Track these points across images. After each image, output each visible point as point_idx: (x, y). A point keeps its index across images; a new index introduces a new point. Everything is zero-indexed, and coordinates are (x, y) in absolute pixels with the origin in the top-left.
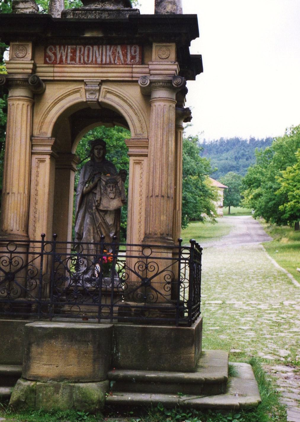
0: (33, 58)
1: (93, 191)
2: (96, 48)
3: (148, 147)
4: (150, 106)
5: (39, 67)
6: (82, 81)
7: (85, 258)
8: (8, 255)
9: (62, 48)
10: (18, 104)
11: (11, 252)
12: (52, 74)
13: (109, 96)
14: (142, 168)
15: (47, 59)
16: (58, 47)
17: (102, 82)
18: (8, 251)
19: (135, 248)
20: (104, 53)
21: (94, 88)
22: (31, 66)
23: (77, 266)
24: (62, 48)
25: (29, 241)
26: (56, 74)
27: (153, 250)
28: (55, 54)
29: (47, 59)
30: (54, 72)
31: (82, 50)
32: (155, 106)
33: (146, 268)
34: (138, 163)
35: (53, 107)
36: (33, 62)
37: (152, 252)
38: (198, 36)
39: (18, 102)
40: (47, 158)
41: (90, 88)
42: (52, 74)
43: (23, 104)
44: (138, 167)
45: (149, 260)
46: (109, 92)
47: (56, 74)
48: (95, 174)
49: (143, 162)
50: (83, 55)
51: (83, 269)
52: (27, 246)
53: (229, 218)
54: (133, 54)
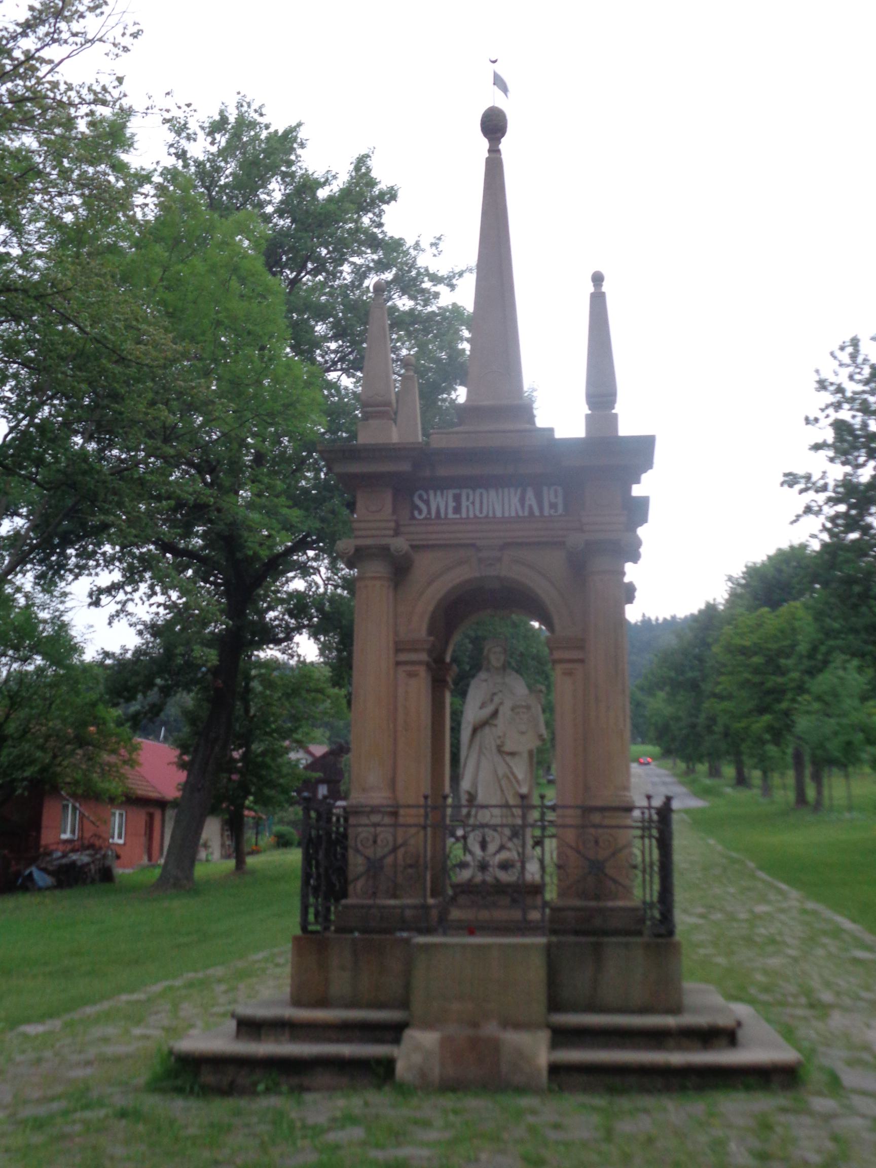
0: (395, 511)
1: (491, 722)
2: (492, 493)
3: (398, 650)
6: (473, 545)
7: (495, 830)
8: (372, 830)
11: (375, 825)
15: (416, 513)
16: (431, 493)
17: (506, 546)
19: (569, 812)
20: (506, 499)
22: (392, 525)
23: (484, 845)
25: (398, 806)
28: (427, 503)
31: (485, 496)
34: (569, 673)
36: (394, 518)
40: (422, 671)
45: (600, 831)
50: (473, 503)
51: (492, 847)
52: (395, 814)
53: (475, 784)
54: (553, 500)
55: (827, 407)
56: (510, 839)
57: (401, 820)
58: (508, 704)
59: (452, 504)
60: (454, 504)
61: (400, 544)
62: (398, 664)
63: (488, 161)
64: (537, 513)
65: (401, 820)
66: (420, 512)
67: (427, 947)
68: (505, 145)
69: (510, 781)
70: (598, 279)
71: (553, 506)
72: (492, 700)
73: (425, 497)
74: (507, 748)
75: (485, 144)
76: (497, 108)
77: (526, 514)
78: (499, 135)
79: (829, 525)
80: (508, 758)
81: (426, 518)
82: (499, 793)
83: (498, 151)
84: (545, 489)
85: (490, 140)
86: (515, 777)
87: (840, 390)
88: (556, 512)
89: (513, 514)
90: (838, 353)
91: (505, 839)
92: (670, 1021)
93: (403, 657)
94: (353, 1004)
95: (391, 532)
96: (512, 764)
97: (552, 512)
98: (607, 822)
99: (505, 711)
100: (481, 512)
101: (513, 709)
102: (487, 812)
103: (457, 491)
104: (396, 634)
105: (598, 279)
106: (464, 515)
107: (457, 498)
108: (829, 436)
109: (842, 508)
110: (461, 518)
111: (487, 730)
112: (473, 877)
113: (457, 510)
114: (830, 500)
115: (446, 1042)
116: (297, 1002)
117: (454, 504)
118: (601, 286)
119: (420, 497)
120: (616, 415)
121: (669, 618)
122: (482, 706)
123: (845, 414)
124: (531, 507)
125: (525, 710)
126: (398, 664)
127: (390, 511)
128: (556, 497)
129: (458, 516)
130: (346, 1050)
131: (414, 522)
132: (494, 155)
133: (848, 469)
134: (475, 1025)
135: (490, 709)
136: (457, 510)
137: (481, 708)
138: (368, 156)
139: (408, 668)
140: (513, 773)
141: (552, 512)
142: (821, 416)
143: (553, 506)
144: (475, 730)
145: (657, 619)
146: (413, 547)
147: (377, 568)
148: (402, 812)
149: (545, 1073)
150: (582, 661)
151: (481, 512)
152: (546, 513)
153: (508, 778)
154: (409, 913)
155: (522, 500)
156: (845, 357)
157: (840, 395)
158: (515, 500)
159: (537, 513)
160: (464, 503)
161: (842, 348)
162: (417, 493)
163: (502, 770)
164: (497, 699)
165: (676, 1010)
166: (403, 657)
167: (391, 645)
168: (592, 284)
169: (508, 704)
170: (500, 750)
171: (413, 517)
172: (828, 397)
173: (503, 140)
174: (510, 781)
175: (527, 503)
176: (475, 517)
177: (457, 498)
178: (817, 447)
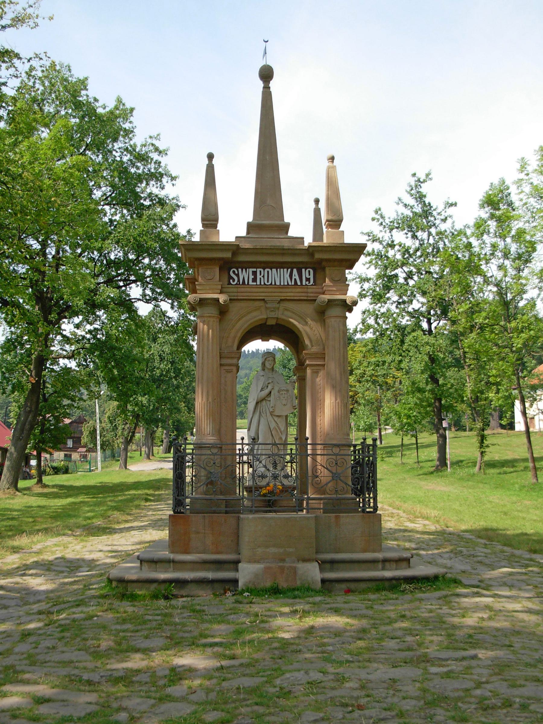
2: (274, 270)
15: (231, 281)
22: (220, 287)
28: (238, 275)
50: (263, 276)
54: (308, 277)
56: (260, 462)
58: (276, 389)
59: (251, 277)
64: (299, 283)
66: (234, 281)
67: (343, 516)
71: (308, 280)
73: (236, 272)
77: (293, 283)
81: (237, 284)
82: (271, 437)
84: (303, 270)
86: (280, 429)
92: (379, 556)
93: (224, 361)
94: (204, 552)
97: (307, 283)
100: (268, 282)
103: (255, 270)
106: (258, 283)
107: (254, 273)
113: (254, 280)
119: (234, 272)
121: (255, 351)
122: (262, 390)
124: (295, 279)
126: (221, 365)
130: (210, 575)
131: (230, 286)
135: (267, 391)
136: (254, 280)
140: (278, 427)
141: (307, 283)
143: (308, 280)
145: (248, 351)
149: (320, 584)
151: (268, 282)
152: (304, 283)
158: (287, 276)
159: (299, 283)
160: (258, 276)
162: (232, 271)
164: (270, 387)
165: (380, 550)
166: (224, 361)
169: (276, 389)
170: (272, 414)
171: (229, 283)
176: (265, 284)
177: (254, 273)
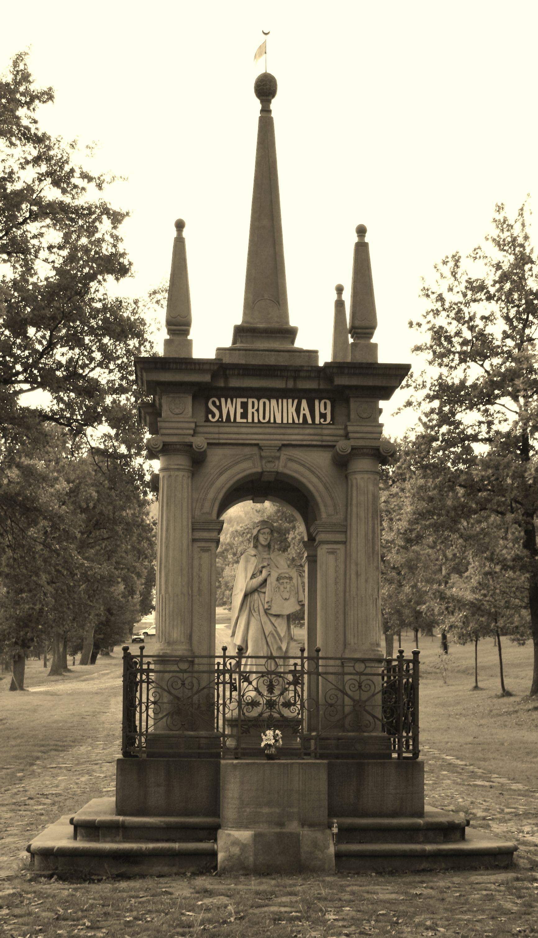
3: (193, 530)
4: (346, 477)
5: (201, 426)
6: (257, 445)
9: (229, 400)
10: (177, 476)
12: (216, 436)
13: (290, 464)
14: (336, 560)
15: (210, 416)
18: (178, 669)
19: (331, 662)
21: (273, 454)
22: (193, 425)
24: (229, 400)
26: (222, 436)
27: (368, 665)
28: (219, 408)
29: (210, 416)
30: (219, 433)
32: (356, 479)
33: (360, 687)
34: (333, 552)
35: (217, 478)
37: (366, 667)
38: (316, 352)
39: (176, 473)
41: (268, 454)
42: (216, 436)
43: (184, 476)
44: (331, 558)
45: (363, 678)
46: (290, 460)
47: (222, 436)
48: (263, 567)
49: (338, 551)
50: (258, 410)
52: (192, 663)
54: (323, 411)
55: (428, 313)
57: (196, 668)
58: (274, 575)
59: (240, 411)
60: (242, 411)
61: (199, 442)
62: (194, 540)
63: (261, 120)
64: (310, 421)
65: (196, 668)
66: (214, 416)
68: (275, 104)
69: (274, 638)
70: (361, 231)
72: (261, 572)
73: (218, 404)
74: (273, 612)
75: (257, 105)
76: (270, 74)
77: (301, 421)
78: (270, 98)
79: (425, 419)
80: (273, 619)
81: (218, 421)
82: (265, 646)
83: (270, 111)
84: (317, 402)
85: (262, 102)
86: (279, 635)
87: (441, 298)
88: (325, 420)
89: (290, 421)
90: (440, 266)
91: (251, 687)
93: (198, 535)
95: (191, 432)
96: (276, 625)
98: (368, 671)
99: (272, 580)
100: (264, 418)
101: (278, 579)
102: (201, 666)
103: (245, 400)
104: (193, 517)
105: (361, 231)
106: (250, 420)
107: (244, 406)
108: (426, 338)
109: (436, 404)
110: (247, 422)
111: (256, 596)
112: (261, 715)
113: (244, 415)
114: (428, 396)
115: (257, 837)
116: (120, 811)
117: (242, 411)
118: (364, 236)
119: (214, 403)
120: (375, 346)
122: (253, 576)
123: (442, 321)
124: (304, 415)
125: (288, 581)
126: (194, 540)
127: (190, 414)
128: (325, 409)
129: (245, 421)
132: (265, 115)
133: (444, 370)
134: (281, 825)
135: (260, 579)
136: (244, 415)
137: (251, 578)
138: (26, 54)
139: (203, 544)
141: (322, 420)
142: (423, 321)
143: (323, 416)
144: (246, 596)
146: (209, 444)
147: (182, 461)
148: (197, 661)
150: (345, 543)
151: (264, 418)
152: (317, 421)
153: (273, 634)
154: (203, 741)
155: (298, 410)
156: (447, 270)
157: (439, 303)
158: (292, 410)
159: (310, 421)
161: (445, 263)
163: (268, 628)
164: (264, 573)
166: (198, 535)
167: (190, 525)
168: (356, 235)
171: (207, 420)
172: (432, 304)
173: (273, 101)
174: (274, 638)
175: (302, 412)
176: (259, 421)
177: (244, 406)
178: (418, 349)
